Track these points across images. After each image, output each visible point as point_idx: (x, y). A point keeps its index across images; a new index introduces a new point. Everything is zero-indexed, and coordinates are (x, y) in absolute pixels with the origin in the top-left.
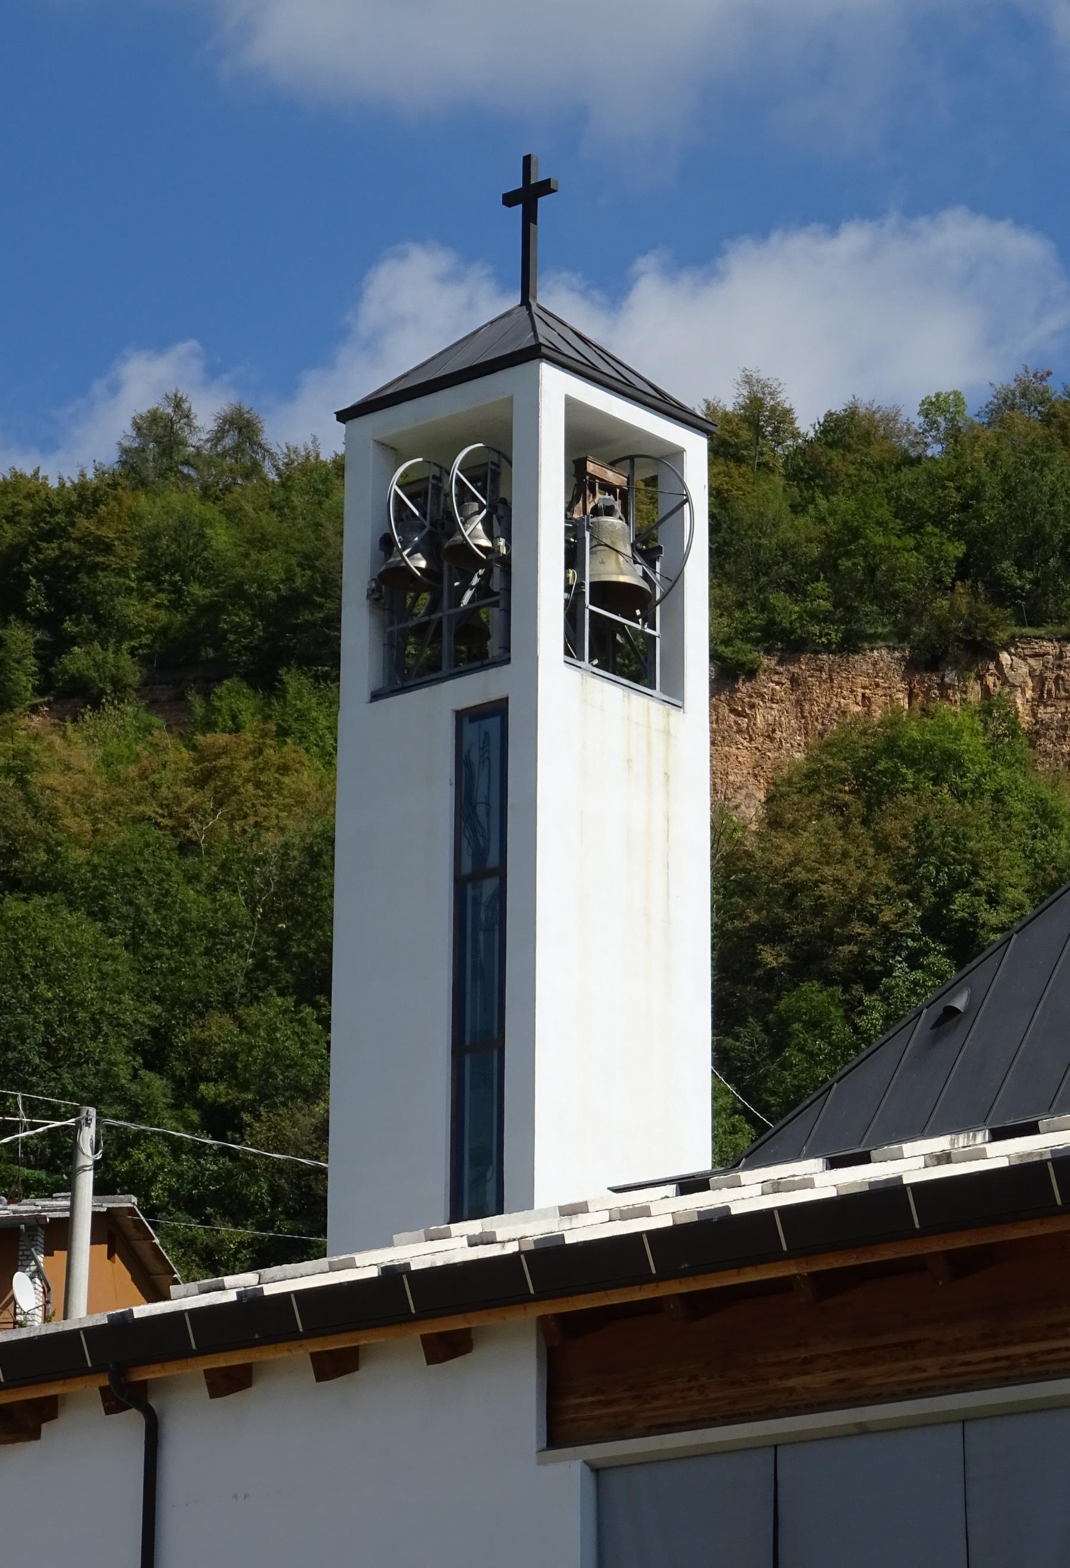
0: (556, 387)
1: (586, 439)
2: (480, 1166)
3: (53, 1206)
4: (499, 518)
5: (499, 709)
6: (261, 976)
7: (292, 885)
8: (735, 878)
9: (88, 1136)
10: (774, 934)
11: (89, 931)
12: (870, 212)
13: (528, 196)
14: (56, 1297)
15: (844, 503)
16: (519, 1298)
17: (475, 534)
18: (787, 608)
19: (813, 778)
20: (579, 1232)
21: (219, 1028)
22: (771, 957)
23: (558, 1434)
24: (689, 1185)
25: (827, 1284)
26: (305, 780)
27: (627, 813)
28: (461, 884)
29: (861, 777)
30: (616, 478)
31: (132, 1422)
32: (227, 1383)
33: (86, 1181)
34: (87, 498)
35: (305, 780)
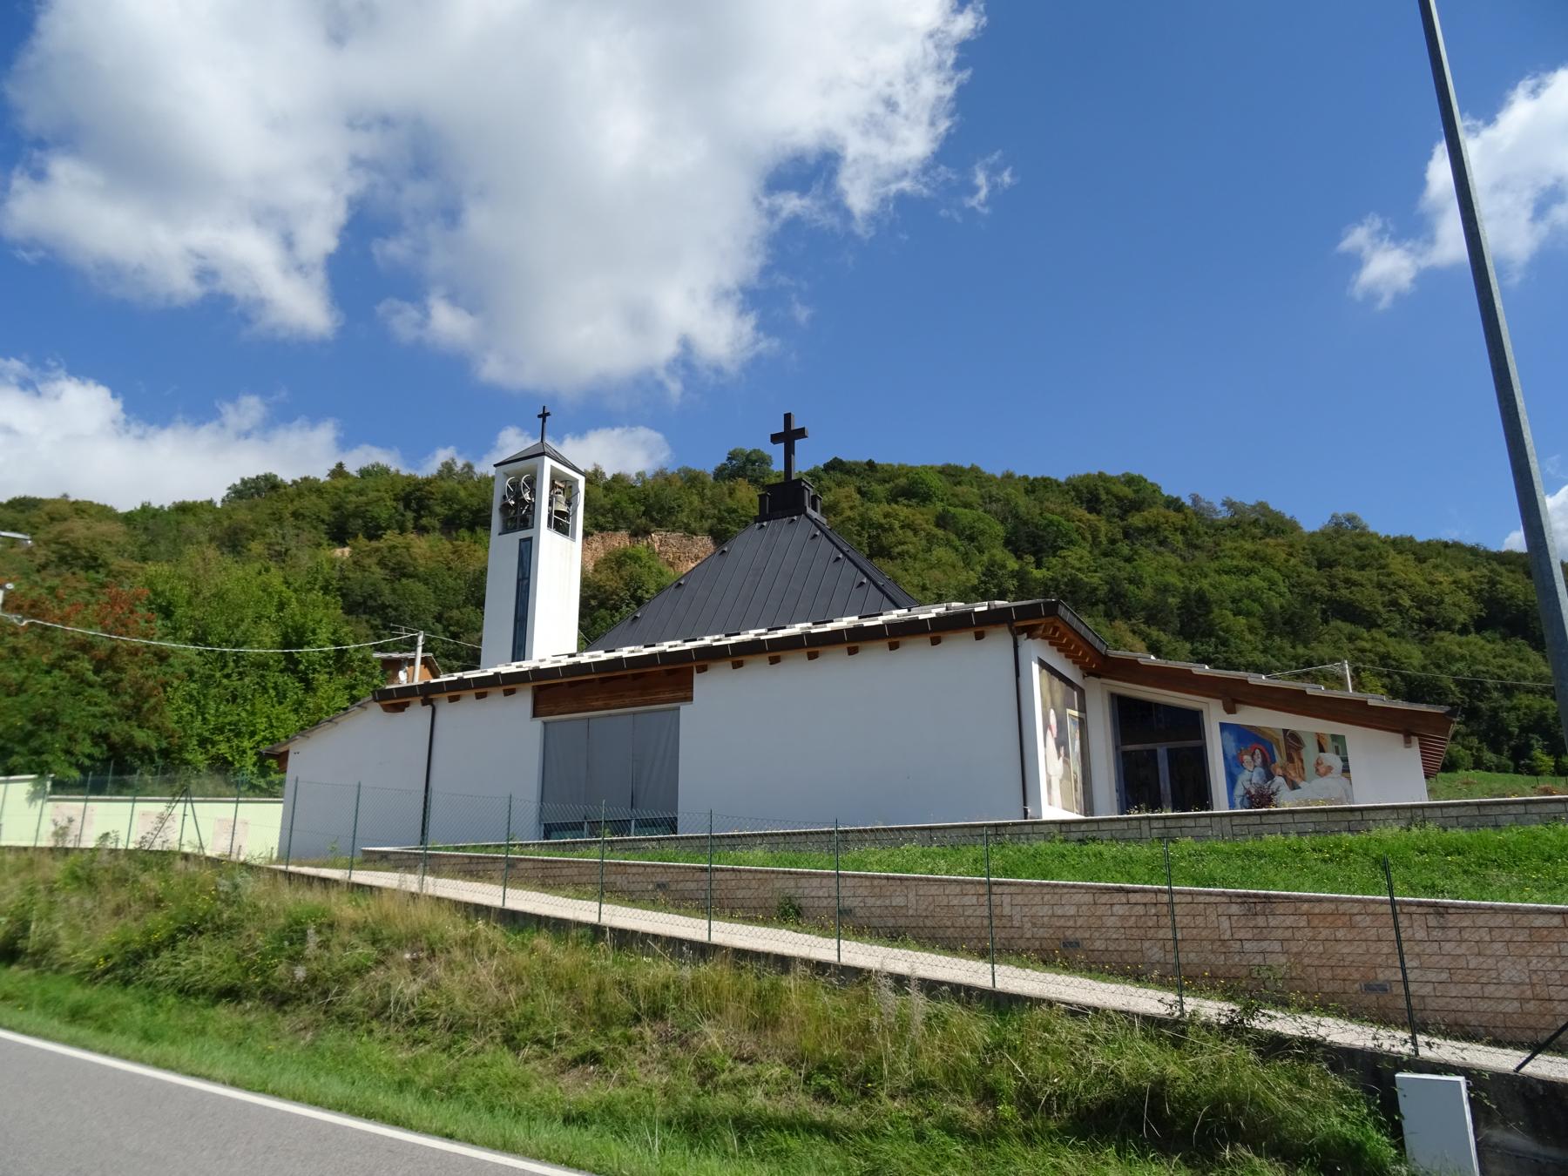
0: (548, 463)
1: (555, 475)
2: (520, 649)
3: (410, 655)
4: (533, 493)
5: (530, 539)
6: (467, 601)
7: (476, 579)
8: (586, 584)
9: (421, 638)
10: (594, 597)
11: (423, 588)
12: (622, 426)
13: (544, 416)
14: (411, 677)
15: (616, 496)
16: (528, 681)
17: (527, 496)
18: (601, 520)
19: (606, 560)
20: (543, 666)
21: (455, 613)
22: (593, 603)
23: (535, 714)
24: (571, 656)
25: (603, 680)
26: (480, 554)
27: (561, 566)
28: (518, 581)
29: (618, 561)
30: (562, 485)
31: (429, 708)
32: (453, 699)
33: (420, 649)
34: (428, 482)
35: (480, 554)
